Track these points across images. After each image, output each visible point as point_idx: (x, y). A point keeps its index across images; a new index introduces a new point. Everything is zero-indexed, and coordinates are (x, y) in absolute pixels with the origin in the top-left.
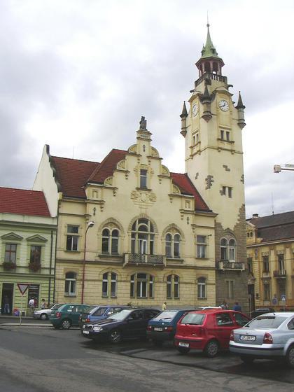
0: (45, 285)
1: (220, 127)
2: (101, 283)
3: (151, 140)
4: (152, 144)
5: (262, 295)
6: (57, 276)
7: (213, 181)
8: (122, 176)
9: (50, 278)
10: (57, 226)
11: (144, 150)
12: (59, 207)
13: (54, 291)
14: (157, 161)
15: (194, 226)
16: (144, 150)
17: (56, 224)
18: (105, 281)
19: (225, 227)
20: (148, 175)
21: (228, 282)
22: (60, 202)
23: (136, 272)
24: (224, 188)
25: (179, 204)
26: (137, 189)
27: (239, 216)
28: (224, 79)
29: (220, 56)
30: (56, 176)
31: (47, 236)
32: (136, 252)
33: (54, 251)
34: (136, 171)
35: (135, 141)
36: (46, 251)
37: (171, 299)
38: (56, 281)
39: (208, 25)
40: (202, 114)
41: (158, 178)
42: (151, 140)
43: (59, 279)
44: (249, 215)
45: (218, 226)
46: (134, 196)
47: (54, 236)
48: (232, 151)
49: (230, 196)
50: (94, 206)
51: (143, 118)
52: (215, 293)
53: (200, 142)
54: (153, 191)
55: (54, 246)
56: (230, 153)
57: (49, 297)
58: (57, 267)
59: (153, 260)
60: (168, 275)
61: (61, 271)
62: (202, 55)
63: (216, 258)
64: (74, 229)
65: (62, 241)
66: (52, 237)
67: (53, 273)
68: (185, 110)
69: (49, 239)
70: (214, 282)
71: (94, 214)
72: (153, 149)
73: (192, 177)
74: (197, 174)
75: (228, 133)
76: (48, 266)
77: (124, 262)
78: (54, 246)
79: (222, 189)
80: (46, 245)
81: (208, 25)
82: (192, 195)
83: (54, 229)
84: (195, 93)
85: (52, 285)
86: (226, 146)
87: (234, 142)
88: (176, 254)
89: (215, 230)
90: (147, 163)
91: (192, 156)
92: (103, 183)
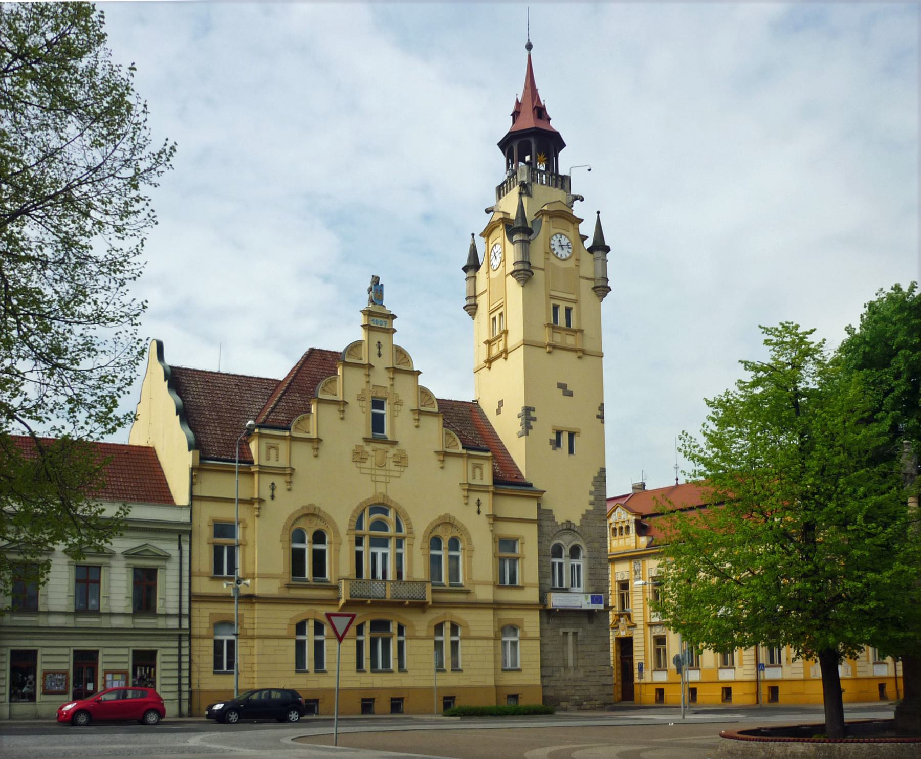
1: (552, 297)
2: (293, 643)
3: (395, 331)
4: (397, 340)
5: (651, 662)
6: (195, 632)
7: (535, 419)
8: (331, 412)
9: (180, 635)
10: (190, 523)
11: (379, 355)
12: (192, 484)
13: (190, 662)
14: (410, 378)
15: (495, 519)
16: (379, 355)
17: (187, 519)
19: (560, 518)
20: (387, 411)
21: (566, 634)
22: (196, 472)
24: (559, 434)
25: (458, 470)
26: (366, 440)
27: (591, 493)
28: (563, 182)
29: (555, 125)
30: (185, 414)
31: (170, 547)
34: (361, 398)
35: (360, 335)
36: (169, 579)
37: (444, 671)
38: (195, 642)
39: (529, 47)
40: (510, 268)
41: (412, 416)
42: (395, 331)
43: (200, 637)
44: (616, 487)
45: (544, 517)
46: (359, 456)
47: (186, 547)
48: (582, 353)
49: (571, 451)
50: (267, 480)
51: (376, 280)
53: (506, 332)
55: (186, 567)
56: (572, 356)
58: (195, 613)
59: (404, 592)
60: (299, 620)
61: (204, 616)
64: (223, 529)
65: (204, 559)
66: (180, 548)
67: (185, 624)
69: (175, 553)
71: (273, 497)
72: (400, 352)
73: (489, 409)
74: (501, 403)
75: (568, 310)
76: (176, 611)
77: (339, 599)
78: (186, 567)
79: (554, 437)
81: (529, 47)
82: (486, 451)
83: (185, 532)
84: (498, 216)
85: (185, 651)
86: (570, 341)
87: (581, 331)
88: (454, 574)
89: (540, 526)
90: (387, 383)
91: (490, 361)
92: (289, 429)
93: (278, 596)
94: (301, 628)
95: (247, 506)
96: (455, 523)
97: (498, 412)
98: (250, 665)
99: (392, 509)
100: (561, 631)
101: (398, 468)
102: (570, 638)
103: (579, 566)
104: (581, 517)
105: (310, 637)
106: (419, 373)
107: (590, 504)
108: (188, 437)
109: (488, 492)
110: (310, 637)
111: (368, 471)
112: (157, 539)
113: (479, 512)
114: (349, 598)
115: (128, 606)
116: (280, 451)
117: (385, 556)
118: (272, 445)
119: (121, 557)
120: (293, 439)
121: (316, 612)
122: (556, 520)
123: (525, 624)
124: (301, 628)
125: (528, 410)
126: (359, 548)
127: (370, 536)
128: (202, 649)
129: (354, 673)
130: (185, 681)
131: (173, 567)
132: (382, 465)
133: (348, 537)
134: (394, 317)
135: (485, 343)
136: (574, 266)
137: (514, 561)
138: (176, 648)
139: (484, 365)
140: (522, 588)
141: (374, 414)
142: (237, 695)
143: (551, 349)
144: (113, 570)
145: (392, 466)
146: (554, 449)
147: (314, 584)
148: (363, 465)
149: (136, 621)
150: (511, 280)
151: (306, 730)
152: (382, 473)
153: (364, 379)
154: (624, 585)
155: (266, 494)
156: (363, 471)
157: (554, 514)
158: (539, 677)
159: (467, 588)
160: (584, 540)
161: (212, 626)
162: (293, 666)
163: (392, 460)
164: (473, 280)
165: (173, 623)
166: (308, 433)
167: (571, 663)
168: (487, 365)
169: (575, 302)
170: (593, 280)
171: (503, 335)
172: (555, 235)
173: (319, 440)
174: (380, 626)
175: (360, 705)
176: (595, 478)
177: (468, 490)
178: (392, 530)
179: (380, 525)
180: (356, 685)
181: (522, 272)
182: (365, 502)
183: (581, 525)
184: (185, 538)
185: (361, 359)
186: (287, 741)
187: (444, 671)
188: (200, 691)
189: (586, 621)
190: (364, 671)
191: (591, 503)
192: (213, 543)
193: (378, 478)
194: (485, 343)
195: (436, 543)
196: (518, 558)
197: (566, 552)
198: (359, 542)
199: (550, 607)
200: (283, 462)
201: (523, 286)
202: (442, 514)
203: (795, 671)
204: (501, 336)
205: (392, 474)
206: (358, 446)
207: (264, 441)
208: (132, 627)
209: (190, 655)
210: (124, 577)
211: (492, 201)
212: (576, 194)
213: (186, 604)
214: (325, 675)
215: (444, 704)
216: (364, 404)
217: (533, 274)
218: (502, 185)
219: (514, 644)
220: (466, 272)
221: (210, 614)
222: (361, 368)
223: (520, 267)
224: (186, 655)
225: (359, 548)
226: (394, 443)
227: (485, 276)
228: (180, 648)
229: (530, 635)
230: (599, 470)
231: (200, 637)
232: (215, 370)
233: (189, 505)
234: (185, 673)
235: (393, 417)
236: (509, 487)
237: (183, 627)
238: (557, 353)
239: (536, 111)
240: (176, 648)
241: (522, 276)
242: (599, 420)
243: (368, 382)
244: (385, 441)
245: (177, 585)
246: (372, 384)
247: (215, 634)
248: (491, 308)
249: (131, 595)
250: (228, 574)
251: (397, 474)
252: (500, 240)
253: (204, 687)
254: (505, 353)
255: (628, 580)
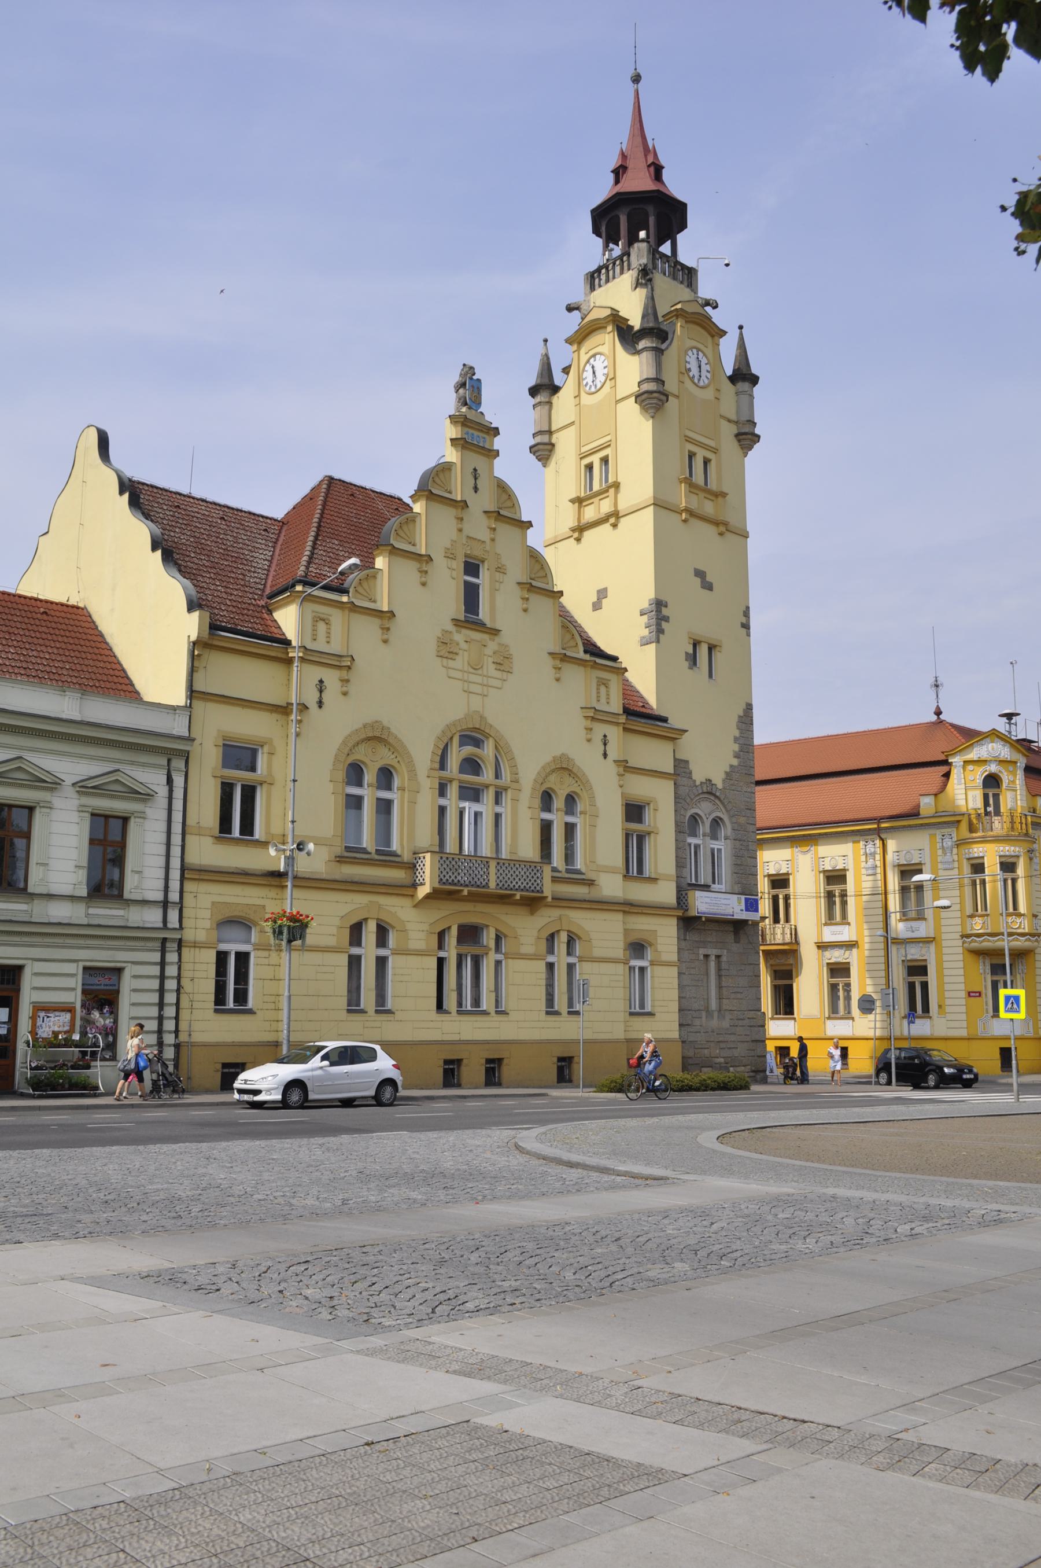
0: (957, 1002)
1: (688, 440)
6: (188, 935)
11: (476, 489)
12: (192, 671)
15: (625, 767)
16: (476, 489)
18: (355, 951)
20: (484, 580)
21: (706, 956)
23: (454, 916)
24: (696, 644)
26: (456, 622)
28: (688, 275)
32: (451, 847)
33: (177, 839)
34: (450, 555)
37: (557, 1013)
39: (637, 79)
41: (517, 592)
43: (195, 945)
45: (681, 767)
47: (179, 780)
50: (315, 673)
52: (675, 994)
53: (616, 486)
54: (505, 637)
55: (177, 817)
56: (711, 530)
57: (161, 1019)
60: (354, 920)
62: (617, 181)
63: (679, 877)
66: (170, 781)
67: (173, 916)
68: (546, 368)
69: (162, 791)
70: (674, 957)
71: (320, 704)
72: (502, 487)
74: (602, 594)
75: (706, 462)
76: (159, 896)
77: (414, 886)
78: (177, 817)
80: (149, 812)
81: (637, 79)
85: (171, 971)
87: (724, 495)
90: (484, 535)
93: (324, 876)
94: (356, 932)
95: (275, 716)
96: (575, 770)
97: (597, 606)
98: (272, 999)
99: (491, 740)
100: (702, 951)
101: (498, 674)
102: (712, 964)
103: (719, 850)
104: (723, 776)
105: (369, 950)
106: (530, 524)
107: (735, 757)
108: (185, 588)
109: (617, 724)
110: (369, 950)
111: (459, 675)
112: (132, 763)
113: (605, 755)
114: (437, 885)
115: (80, 883)
116: (333, 628)
117: (477, 815)
118: (322, 616)
119: (71, 792)
120: (353, 608)
121: (380, 907)
122: (694, 778)
123: (660, 940)
124: (356, 932)
125: (659, 604)
126: (443, 802)
127: (460, 781)
128: (197, 967)
129: (433, 1014)
130: (169, 1025)
131: (156, 813)
132: (476, 667)
133: (428, 781)
134: (496, 431)
135: (573, 501)
136: (713, 398)
137: (641, 839)
138: (155, 964)
139: (571, 533)
140: (653, 880)
141: (466, 583)
142: (289, 1050)
143: (688, 517)
144: (55, 815)
145: (491, 669)
146: (690, 668)
147: (377, 857)
148: (451, 663)
149: (91, 911)
150: (631, 408)
151: (740, 1115)
152: (478, 679)
153: (453, 524)
154: (780, 882)
155: (311, 697)
156: (453, 673)
157: (691, 767)
158: (676, 1026)
159: (590, 875)
160: (727, 811)
161: (215, 926)
162: (343, 1002)
163: (491, 660)
164: (547, 407)
165: (153, 917)
166: (375, 601)
167: (714, 1005)
168: (576, 535)
169: (715, 451)
170: (736, 423)
171: (612, 491)
172: (691, 348)
173: (391, 614)
174: (469, 934)
175: (442, 1070)
176: (740, 717)
177: (593, 719)
178: (488, 775)
179: (472, 765)
180: (436, 1036)
181: (655, 395)
182: (454, 724)
183: (724, 788)
184: (178, 764)
185: (450, 492)
186: (708, 1139)
187: (557, 1013)
188: (193, 1045)
189: (731, 937)
190: (448, 1012)
191: (737, 756)
192: (222, 777)
193: (474, 688)
194: (573, 501)
195: (547, 799)
196: (649, 833)
197: (705, 827)
198: (442, 791)
199: (693, 913)
200: (336, 647)
201: (653, 417)
202: (558, 753)
203: (952, 1024)
204: (607, 491)
205: (492, 682)
206: (446, 632)
207: (311, 607)
208: (85, 921)
209: (179, 978)
210: (74, 829)
211: (577, 291)
212: (708, 297)
213: (175, 885)
214: (389, 1017)
215: (445, 1071)
216: (454, 564)
217: (667, 401)
218: (598, 270)
219: (642, 969)
220: (533, 397)
221: (213, 903)
222: (451, 506)
223: (651, 386)
224: (172, 978)
225: (443, 802)
226: (495, 632)
227: (572, 402)
228: (163, 964)
229: (665, 957)
230: (744, 706)
231: (195, 945)
232: (185, 491)
233: (186, 706)
234: (170, 1012)
235: (494, 590)
236: (639, 720)
237: (169, 925)
238: (693, 521)
239: (652, 169)
240: (155, 964)
241: (655, 401)
242: (744, 630)
243: (460, 530)
244: (480, 626)
245: (162, 849)
246: (466, 532)
247: (220, 941)
248: (584, 450)
249: (85, 862)
250: (241, 834)
251: (498, 683)
252: (605, 349)
253: (198, 1037)
254: (614, 517)
255: (788, 874)
